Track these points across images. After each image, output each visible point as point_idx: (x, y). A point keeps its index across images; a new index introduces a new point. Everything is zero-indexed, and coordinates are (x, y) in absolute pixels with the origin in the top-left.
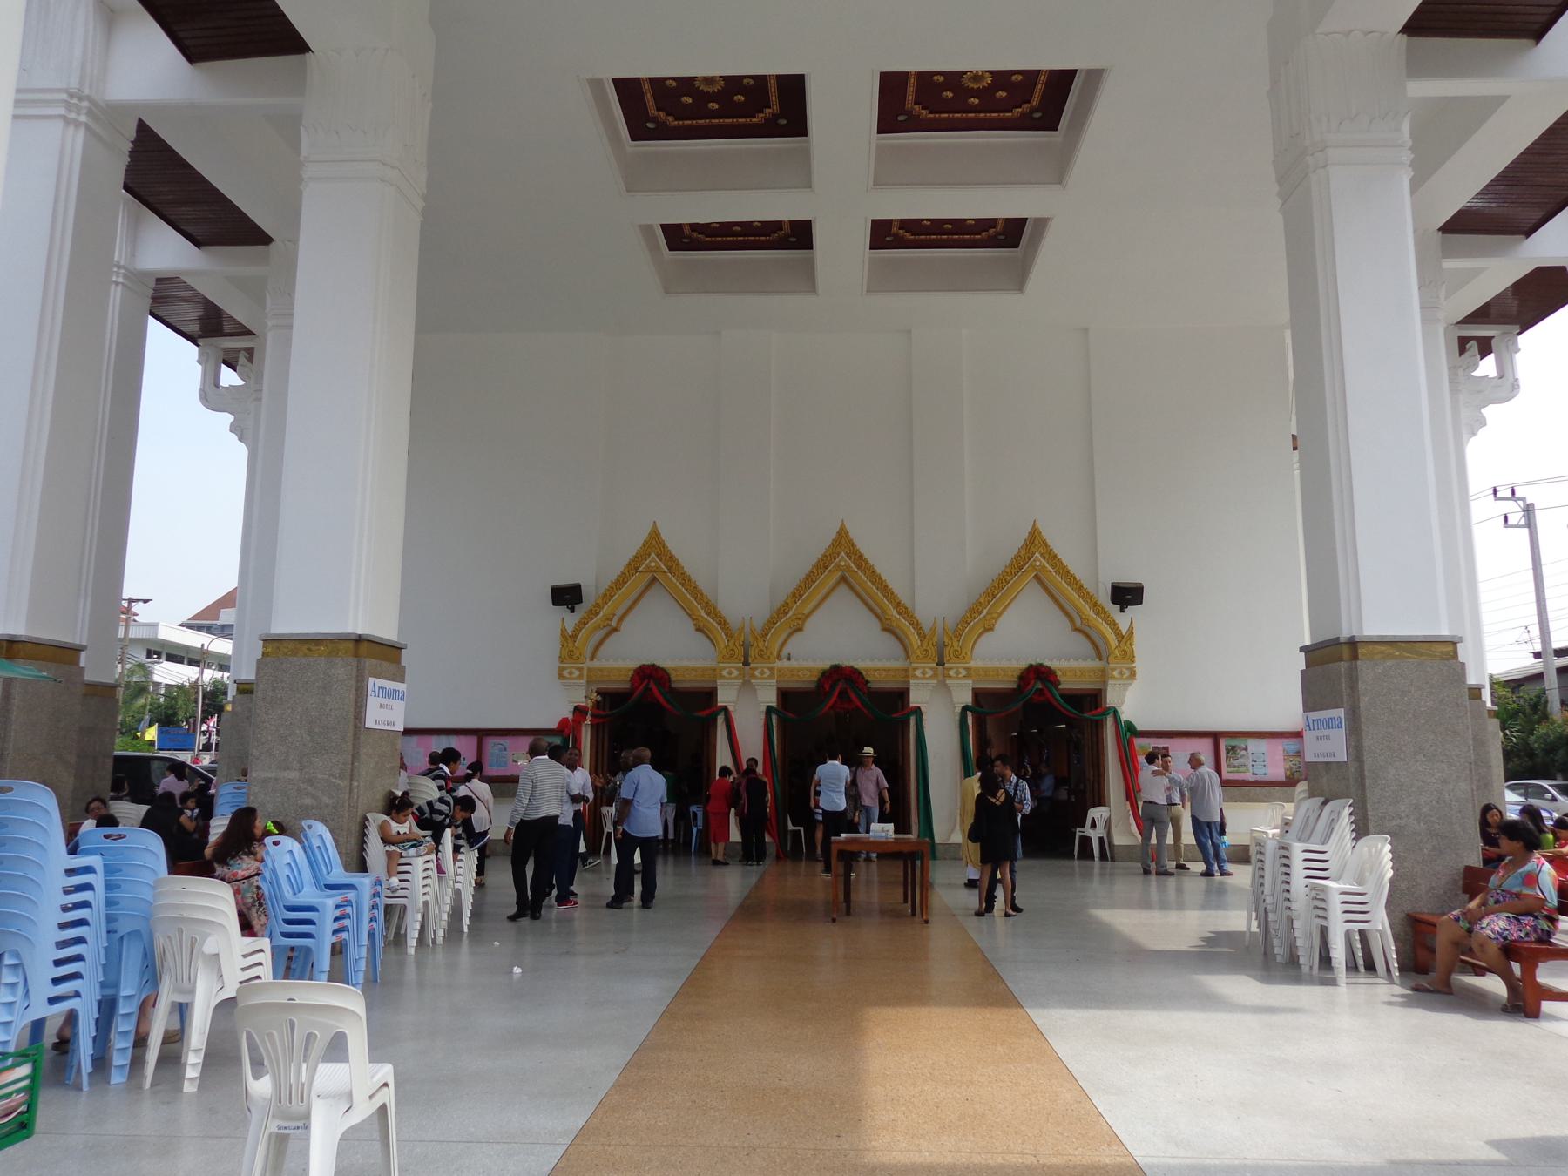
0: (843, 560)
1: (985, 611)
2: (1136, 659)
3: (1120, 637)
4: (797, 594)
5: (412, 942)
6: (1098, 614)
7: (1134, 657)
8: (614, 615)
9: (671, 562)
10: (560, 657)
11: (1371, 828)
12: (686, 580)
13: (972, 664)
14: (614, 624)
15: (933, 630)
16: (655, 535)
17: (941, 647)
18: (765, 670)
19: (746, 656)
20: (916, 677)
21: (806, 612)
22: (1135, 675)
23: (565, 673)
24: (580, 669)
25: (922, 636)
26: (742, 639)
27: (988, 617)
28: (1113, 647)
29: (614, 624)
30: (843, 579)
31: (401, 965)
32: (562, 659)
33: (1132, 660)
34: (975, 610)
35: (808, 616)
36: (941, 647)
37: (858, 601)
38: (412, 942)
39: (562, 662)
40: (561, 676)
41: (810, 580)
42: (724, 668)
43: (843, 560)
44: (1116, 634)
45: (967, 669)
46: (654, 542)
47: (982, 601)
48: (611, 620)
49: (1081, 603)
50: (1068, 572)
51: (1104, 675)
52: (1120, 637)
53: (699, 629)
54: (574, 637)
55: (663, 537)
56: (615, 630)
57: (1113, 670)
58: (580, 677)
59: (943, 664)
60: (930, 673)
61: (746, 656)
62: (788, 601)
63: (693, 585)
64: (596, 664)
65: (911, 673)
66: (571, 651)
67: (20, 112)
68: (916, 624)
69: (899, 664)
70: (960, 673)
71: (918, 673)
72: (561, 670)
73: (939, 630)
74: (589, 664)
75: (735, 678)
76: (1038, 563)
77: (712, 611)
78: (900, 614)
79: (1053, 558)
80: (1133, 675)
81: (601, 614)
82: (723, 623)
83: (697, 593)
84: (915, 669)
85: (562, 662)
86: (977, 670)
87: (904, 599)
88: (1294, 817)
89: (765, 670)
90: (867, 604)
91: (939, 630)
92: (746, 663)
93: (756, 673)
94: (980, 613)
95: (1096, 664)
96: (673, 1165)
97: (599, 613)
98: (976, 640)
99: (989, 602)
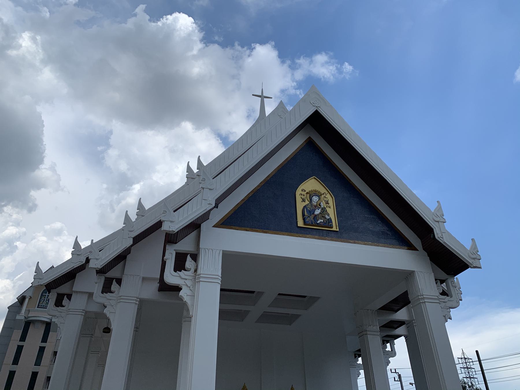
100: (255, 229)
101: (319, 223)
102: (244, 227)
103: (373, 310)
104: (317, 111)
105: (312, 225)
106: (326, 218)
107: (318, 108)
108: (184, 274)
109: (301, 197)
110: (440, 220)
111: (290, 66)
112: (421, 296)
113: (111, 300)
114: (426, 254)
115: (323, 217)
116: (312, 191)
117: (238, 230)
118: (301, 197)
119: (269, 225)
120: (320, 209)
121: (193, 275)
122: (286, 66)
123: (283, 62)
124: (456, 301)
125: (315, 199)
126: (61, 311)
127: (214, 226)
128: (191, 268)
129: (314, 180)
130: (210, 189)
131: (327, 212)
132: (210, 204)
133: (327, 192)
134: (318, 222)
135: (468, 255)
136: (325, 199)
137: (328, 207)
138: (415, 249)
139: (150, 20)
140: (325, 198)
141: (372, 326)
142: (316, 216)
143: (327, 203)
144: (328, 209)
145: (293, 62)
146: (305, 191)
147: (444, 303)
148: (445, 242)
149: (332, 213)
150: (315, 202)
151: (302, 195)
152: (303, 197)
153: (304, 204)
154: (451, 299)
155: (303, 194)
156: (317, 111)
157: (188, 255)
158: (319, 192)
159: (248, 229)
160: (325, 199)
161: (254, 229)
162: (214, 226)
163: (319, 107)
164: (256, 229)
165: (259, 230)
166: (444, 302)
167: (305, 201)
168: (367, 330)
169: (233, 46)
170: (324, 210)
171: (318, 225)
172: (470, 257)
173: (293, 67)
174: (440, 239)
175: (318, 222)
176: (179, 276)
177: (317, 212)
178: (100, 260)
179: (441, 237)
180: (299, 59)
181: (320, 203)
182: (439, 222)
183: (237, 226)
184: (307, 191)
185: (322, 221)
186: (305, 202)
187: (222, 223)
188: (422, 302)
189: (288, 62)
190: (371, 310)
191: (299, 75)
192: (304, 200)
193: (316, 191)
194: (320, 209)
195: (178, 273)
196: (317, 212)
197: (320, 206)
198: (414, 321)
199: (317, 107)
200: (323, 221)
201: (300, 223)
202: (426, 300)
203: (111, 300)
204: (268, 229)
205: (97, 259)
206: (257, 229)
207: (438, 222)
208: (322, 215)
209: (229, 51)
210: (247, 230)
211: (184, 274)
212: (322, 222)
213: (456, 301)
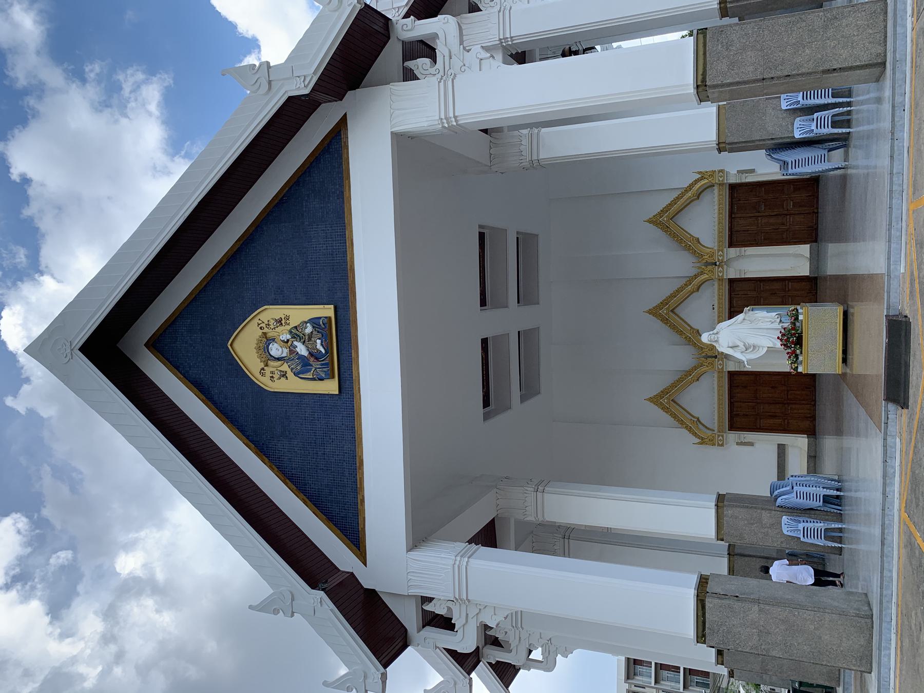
0: (664, 312)
1: (690, 243)
2: (714, 170)
3: (702, 178)
4: (681, 333)
5: (838, 493)
6: (691, 189)
7: (712, 171)
8: (691, 419)
9: (664, 392)
10: (712, 445)
11: (792, 135)
12: (673, 385)
13: (716, 248)
14: (696, 420)
15: (699, 268)
16: (650, 312)
17: (707, 264)
18: (719, 254)
19: (712, 357)
20: (723, 180)
21: (689, 328)
22: (722, 170)
23: (720, 443)
24: (719, 436)
25: (702, 273)
26: (703, 267)
27: (692, 242)
28: (708, 181)
29: (696, 420)
30: (672, 311)
31: (848, 529)
32: (714, 445)
33: (714, 172)
34: (688, 248)
35: (691, 327)
36: (707, 264)
37: (684, 210)
38: (838, 493)
39: (715, 445)
40: (722, 445)
41: (673, 327)
42: (718, 275)
43: (664, 312)
44: (701, 180)
45: (719, 251)
46: (655, 400)
47: (684, 245)
48: (694, 421)
49: (685, 197)
50: (670, 204)
51: (721, 184)
52: (702, 178)
53: (698, 289)
54: (702, 439)
55: (652, 396)
56: (698, 419)
57: (719, 180)
58: (722, 436)
59: (716, 356)
60: (720, 362)
61: (712, 357)
62: (684, 337)
63: (676, 382)
64: (716, 429)
65: (721, 182)
66: (709, 440)
67: (404, 43)
68: (696, 276)
69: (716, 189)
70: (721, 270)
71: (720, 275)
72: (719, 445)
73: (698, 265)
74: (716, 431)
75: (723, 363)
76: (665, 219)
77: (688, 373)
78: (691, 284)
79: (663, 211)
80: (721, 171)
81: (691, 425)
82: (695, 368)
83: (680, 380)
84: (718, 276)
85: (715, 445)
86: (719, 246)
87: (684, 281)
88: (786, 688)
89: (719, 254)
90: (686, 298)
91: (698, 265)
92: (716, 357)
93: (720, 258)
94: (690, 246)
95: (716, 189)
96: (920, 129)
97: (690, 337)
98: (704, 246)
99: (685, 241)
100: (358, 483)
101: (324, 348)
102: (357, 506)
103: (491, 142)
104: (83, 349)
105: (330, 364)
106: (312, 332)
107: (75, 347)
108: (458, 619)
109: (277, 379)
110: (265, 79)
111: (40, 98)
112: (443, 123)
113: (520, 638)
114: (350, 94)
115: (310, 339)
116: (260, 357)
117: (364, 518)
118: (277, 379)
119: (346, 453)
120: (295, 343)
121: (458, 604)
122: (41, 108)
123: (36, 115)
124: (444, 23)
125: (276, 350)
126: (547, 651)
127: (365, 565)
128: (447, 606)
129: (236, 345)
130: (293, 600)
131: (299, 325)
132: (321, 602)
133: (256, 321)
134: (323, 351)
135: (335, 11)
136: (272, 327)
137: (288, 322)
138: (343, 121)
139: (27, 380)
140: (269, 325)
141: (522, 148)
142: (311, 354)
143: (279, 322)
144: (294, 322)
145: (26, 92)
146: (263, 369)
147: (453, 57)
148: (315, 73)
149: (300, 314)
150: (283, 350)
151: (272, 377)
152: (276, 376)
153: (290, 374)
154: (441, 35)
155: (271, 375)
156: (83, 349)
157: (425, 610)
158: (259, 341)
159: (360, 497)
160: (272, 327)
161: (358, 486)
162: (365, 565)
163: (71, 345)
164: (358, 481)
165: (358, 474)
166: (451, 58)
167: (284, 373)
168: (530, 159)
169: (31, 219)
170: (296, 334)
171: (329, 350)
172: (339, 9)
173: (39, 89)
174: (309, 82)
175: (323, 351)
176: (462, 628)
177: (302, 350)
178: (456, 679)
179: (304, 81)
180: (17, 78)
181: (283, 341)
182: (270, 81)
183: (358, 519)
184: (262, 365)
185: (319, 341)
186: (286, 372)
187: (356, 547)
188: (456, 121)
189: (31, 101)
190: (491, 148)
191: (53, 76)
192: (284, 375)
193: (258, 348)
194: (295, 343)
195: (459, 629)
196: (302, 350)
197: (288, 341)
198: (504, 44)
199: (72, 350)
200: (319, 339)
201: (331, 387)
202: (451, 115)
203: (520, 638)
204: (354, 457)
205: (455, 684)
206: (358, 479)
207: (270, 82)
208: (306, 341)
209: (45, 224)
210: (363, 501)
211: (458, 619)
212: (322, 342)
213: (444, 23)
